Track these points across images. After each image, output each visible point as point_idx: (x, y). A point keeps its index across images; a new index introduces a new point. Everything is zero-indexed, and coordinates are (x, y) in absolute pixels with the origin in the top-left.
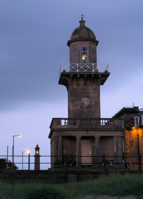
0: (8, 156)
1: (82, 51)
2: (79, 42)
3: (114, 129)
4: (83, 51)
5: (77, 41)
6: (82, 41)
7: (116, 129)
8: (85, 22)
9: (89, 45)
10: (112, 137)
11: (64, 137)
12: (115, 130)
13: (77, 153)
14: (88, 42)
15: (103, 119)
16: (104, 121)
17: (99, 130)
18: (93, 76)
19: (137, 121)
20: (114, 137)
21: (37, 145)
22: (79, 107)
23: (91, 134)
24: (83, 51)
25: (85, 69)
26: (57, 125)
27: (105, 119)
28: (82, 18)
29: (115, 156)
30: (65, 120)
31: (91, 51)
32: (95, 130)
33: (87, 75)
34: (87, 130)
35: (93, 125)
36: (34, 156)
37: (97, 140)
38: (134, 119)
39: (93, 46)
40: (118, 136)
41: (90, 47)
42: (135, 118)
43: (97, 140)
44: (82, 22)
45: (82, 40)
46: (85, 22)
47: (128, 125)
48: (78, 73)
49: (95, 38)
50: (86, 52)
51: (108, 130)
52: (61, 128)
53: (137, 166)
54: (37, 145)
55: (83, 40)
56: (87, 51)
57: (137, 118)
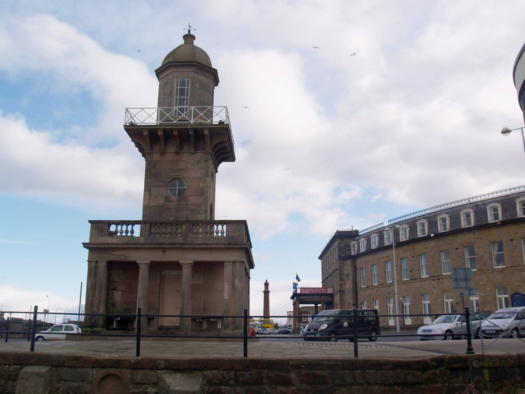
2: (172, 70)
3: (224, 244)
4: (179, 88)
7: (228, 244)
10: (220, 264)
11: (110, 264)
12: (226, 246)
13: (138, 300)
14: (192, 69)
18: (191, 133)
19: (355, 247)
20: (225, 264)
21: (267, 280)
22: (162, 201)
23: (171, 256)
28: (189, 31)
29: (179, 314)
30: (127, 226)
31: (197, 86)
32: (181, 248)
33: (179, 130)
34: (163, 249)
37: (186, 271)
38: (351, 245)
40: (234, 262)
42: (352, 244)
43: (186, 271)
44: (189, 38)
45: (177, 64)
47: (343, 253)
48: (159, 127)
50: (186, 88)
54: (267, 280)
55: (179, 64)
56: (188, 86)
57: (354, 244)
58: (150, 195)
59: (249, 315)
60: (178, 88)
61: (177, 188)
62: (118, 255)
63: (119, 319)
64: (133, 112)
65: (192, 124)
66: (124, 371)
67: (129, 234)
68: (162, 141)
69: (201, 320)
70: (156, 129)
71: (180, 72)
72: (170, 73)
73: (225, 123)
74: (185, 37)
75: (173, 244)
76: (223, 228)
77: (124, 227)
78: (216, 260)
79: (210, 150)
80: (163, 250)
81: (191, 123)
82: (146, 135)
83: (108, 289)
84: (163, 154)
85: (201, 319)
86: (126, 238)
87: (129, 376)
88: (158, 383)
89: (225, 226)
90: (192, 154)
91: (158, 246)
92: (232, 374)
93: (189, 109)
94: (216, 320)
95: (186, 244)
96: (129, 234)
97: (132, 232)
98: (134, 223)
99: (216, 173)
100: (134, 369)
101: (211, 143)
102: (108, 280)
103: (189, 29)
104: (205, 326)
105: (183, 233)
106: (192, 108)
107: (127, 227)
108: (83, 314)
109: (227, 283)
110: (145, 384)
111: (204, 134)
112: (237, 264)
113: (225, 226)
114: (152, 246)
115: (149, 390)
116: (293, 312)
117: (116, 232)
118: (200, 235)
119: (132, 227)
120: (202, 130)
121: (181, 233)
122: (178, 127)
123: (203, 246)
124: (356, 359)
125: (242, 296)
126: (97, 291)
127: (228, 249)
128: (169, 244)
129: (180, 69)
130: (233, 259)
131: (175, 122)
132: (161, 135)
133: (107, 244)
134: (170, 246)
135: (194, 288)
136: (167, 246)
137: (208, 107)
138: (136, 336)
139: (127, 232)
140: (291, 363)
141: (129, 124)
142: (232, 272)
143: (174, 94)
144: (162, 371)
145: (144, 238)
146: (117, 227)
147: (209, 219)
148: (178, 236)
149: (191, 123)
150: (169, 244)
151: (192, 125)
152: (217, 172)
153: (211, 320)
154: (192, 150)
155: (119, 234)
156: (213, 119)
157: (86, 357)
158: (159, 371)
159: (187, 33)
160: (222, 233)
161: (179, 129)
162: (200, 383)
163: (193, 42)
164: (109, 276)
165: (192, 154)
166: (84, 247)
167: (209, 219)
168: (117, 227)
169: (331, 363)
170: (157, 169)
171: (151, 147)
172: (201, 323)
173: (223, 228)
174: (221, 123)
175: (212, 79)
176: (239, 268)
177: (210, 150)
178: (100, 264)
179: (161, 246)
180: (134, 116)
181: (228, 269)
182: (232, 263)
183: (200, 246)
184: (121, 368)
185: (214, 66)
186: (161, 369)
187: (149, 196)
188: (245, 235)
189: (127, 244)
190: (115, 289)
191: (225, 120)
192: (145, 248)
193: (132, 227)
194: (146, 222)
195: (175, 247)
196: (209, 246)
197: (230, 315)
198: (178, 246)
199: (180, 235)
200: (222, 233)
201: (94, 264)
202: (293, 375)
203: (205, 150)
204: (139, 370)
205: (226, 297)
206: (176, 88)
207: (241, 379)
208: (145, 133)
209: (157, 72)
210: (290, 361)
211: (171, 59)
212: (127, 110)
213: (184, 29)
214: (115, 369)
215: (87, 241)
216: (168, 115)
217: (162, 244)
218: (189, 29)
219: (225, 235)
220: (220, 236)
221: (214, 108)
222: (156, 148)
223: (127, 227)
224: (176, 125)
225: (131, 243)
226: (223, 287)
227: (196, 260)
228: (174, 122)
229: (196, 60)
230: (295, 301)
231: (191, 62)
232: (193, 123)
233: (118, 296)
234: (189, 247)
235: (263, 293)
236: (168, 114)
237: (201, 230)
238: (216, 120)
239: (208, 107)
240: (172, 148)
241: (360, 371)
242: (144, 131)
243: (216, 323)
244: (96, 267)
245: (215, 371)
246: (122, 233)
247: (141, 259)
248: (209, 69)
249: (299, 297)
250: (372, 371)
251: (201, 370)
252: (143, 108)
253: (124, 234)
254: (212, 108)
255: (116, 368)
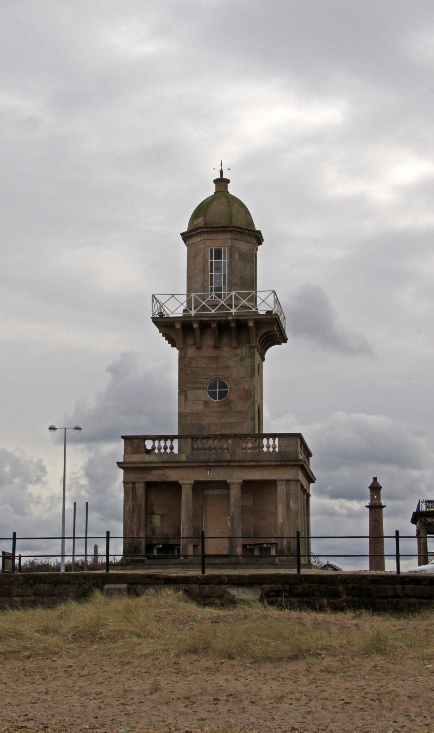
0: (74, 538)
1: (211, 258)
2: (205, 236)
5: (200, 233)
6: (212, 232)
8: (228, 181)
9: (229, 243)
10: (273, 483)
11: (149, 485)
12: (279, 463)
14: (229, 236)
15: (269, 436)
16: (271, 440)
17: (237, 464)
18: (233, 325)
20: (278, 482)
21: (375, 479)
24: (214, 261)
25: (214, 306)
26: (133, 453)
27: (274, 436)
28: (221, 172)
31: (237, 256)
35: (226, 451)
36: (295, 538)
37: (235, 491)
39: (243, 246)
40: (288, 481)
41: (231, 249)
43: (235, 491)
45: (210, 230)
46: (228, 181)
48: (194, 319)
49: (251, 223)
50: (223, 260)
51: (261, 466)
52: (142, 463)
53: (105, 558)
54: (375, 479)
55: (213, 230)
56: (225, 258)
58: (186, 400)
59: (178, 441)
60: (213, 262)
61: (218, 390)
62: (157, 474)
63: (161, 546)
64: (162, 299)
65: (233, 314)
66: (193, 586)
67: (168, 451)
68: (197, 333)
69: (252, 547)
70: (191, 321)
71: (214, 239)
72: (201, 241)
73: (273, 313)
74: (216, 181)
75: (220, 462)
76: (274, 442)
77: (169, 443)
78: (267, 478)
79: (256, 343)
80: (208, 468)
81: (232, 313)
82: (178, 329)
83: (146, 514)
84: (199, 348)
85: (252, 546)
86: (165, 455)
87: (198, 591)
88: (223, 596)
89: (277, 439)
90: (234, 348)
91: (202, 464)
92: (287, 587)
93: (228, 295)
94: (269, 546)
95: (234, 462)
96: (168, 451)
97: (172, 448)
98: (172, 438)
99: (263, 362)
100: (200, 584)
101: (257, 336)
102: (146, 503)
103: (222, 169)
104: (257, 553)
105: (230, 448)
106: (233, 293)
107: (165, 443)
108: (144, 538)
109: (281, 504)
110: (211, 597)
111: (249, 326)
112: (291, 483)
113: (277, 439)
114: (195, 464)
115: (216, 602)
116: (368, 539)
117: (154, 448)
118: (250, 451)
119: (172, 443)
120: (246, 322)
121: (227, 449)
122: (218, 319)
123: (252, 463)
124: (398, 575)
125: (298, 519)
126: (136, 515)
127: (281, 466)
128: (215, 462)
129: (213, 236)
130: (286, 477)
131: (213, 311)
132: (197, 328)
133: (146, 463)
134: (216, 464)
135: (243, 509)
136: (213, 464)
137: (252, 292)
138: (200, 556)
139: (165, 448)
140: (338, 577)
141: (159, 315)
142: (287, 492)
143: (208, 270)
144: (226, 586)
145: (185, 454)
146: (154, 443)
147: (257, 432)
148: (224, 451)
149: (232, 313)
150: (215, 462)
151: (234, 315)
152: (264, 360)
153: (264, 546)
154: (234, 344)
155: (156, 451)
156: (187, 298)
157: (159, 575)
158: (223, 586)
159: (219, 177)
160: (274, 448)
161: (218, 320)
162: (260, 594)
163: (226, 188)
164: (147, 498)
165: (234, 348)
166: (118, 466)
167: (257, 432)
168: (154, 443)
169: (374, 578)
170: (193, 367)
171: (184, 339)
172: (252, 550)
173: (274, 442)
174: (269, 312)
175: (254, 243)
176: (295, 488)
177: (256, 343)
178: (137, 485)
179: (205, 464)
180: (163, 304)
181: (281, 489)
182: (285, 482)
183: (250, 464)
184: (190, 584)
185: (257, 228)
186: (225, 584)
187: (185, 401)
188: (301, 446)
189: (167, 462)
190: (153, 513)
191: (273, 307)
192: (188, 467)
193: (172, 443)
194: (187, 437)
195: (222, 464)
196: (259, 464)
197: (285, 536)
198: (224, 464)
199: (226, 451)
200: (274, 448)
201: (131, 486)
202: (341, 588)
203: (250, 343)
204: (205, 585)
205: (280, 520)
206: (210, 261)
207: (295, 592)
208: (178, 326)
209: (183, 236)
210: (338, 576)
211: (200, 221)
212: (153, 296)
213: (215, 169)
214: (185, 584)
215: (122, 460)
216: (204, 303)
217: (206, 462)
218: (222, 169)
219: (277, 450)
220: (271, 451)
221: (258, 292)
222: (190, 341)
223: (165, 443)
224: (214, 316)
225: (171, 460)
226: (276, 509)
227: (245, 479)
228: (211, 311)
229: (234, 225)
230: (419, 528)
231: (229, 227)
232: (235, 313)
233: (157, 520)
234: (237, 464)
235: (368, 509)
236: (204, 301)
237: (250, 445)
238: (262, 309)
239: (252, 292)
240: (209, 341)
241: (400, 585)
242: (176, 324)
243: (269, 549)
244: (134, 489)
245: (272, 585)
246: (159, 449)
247: (183, 479)
248: (251, 233)
249: (425, 520)
250: (412, 586)
251: (260, 584)
252: (173, 295)
253: (162, 451)
254: (256, 293)
255: (186, 583)
